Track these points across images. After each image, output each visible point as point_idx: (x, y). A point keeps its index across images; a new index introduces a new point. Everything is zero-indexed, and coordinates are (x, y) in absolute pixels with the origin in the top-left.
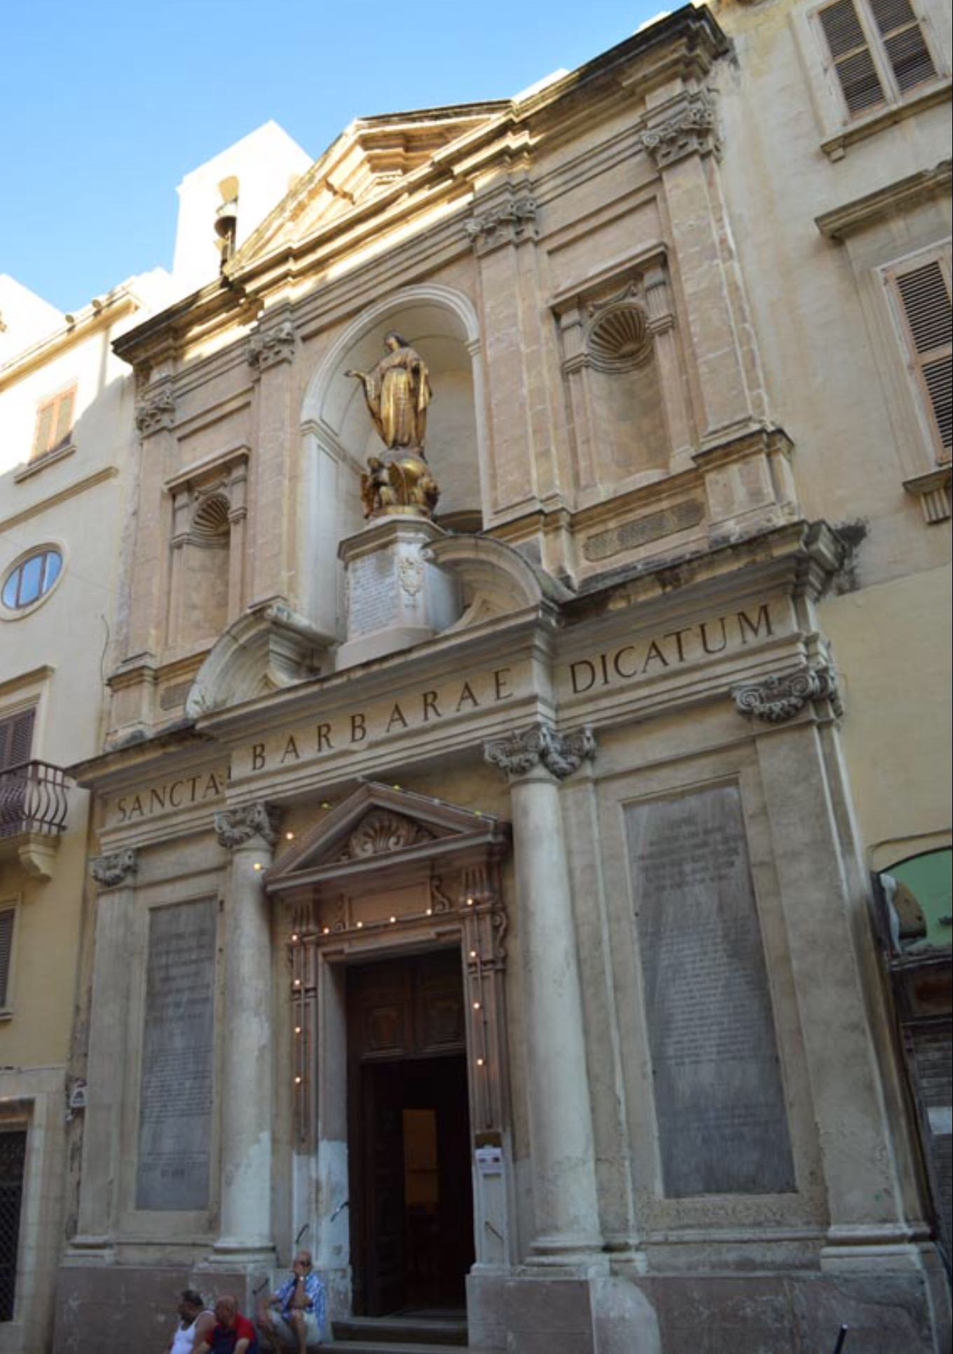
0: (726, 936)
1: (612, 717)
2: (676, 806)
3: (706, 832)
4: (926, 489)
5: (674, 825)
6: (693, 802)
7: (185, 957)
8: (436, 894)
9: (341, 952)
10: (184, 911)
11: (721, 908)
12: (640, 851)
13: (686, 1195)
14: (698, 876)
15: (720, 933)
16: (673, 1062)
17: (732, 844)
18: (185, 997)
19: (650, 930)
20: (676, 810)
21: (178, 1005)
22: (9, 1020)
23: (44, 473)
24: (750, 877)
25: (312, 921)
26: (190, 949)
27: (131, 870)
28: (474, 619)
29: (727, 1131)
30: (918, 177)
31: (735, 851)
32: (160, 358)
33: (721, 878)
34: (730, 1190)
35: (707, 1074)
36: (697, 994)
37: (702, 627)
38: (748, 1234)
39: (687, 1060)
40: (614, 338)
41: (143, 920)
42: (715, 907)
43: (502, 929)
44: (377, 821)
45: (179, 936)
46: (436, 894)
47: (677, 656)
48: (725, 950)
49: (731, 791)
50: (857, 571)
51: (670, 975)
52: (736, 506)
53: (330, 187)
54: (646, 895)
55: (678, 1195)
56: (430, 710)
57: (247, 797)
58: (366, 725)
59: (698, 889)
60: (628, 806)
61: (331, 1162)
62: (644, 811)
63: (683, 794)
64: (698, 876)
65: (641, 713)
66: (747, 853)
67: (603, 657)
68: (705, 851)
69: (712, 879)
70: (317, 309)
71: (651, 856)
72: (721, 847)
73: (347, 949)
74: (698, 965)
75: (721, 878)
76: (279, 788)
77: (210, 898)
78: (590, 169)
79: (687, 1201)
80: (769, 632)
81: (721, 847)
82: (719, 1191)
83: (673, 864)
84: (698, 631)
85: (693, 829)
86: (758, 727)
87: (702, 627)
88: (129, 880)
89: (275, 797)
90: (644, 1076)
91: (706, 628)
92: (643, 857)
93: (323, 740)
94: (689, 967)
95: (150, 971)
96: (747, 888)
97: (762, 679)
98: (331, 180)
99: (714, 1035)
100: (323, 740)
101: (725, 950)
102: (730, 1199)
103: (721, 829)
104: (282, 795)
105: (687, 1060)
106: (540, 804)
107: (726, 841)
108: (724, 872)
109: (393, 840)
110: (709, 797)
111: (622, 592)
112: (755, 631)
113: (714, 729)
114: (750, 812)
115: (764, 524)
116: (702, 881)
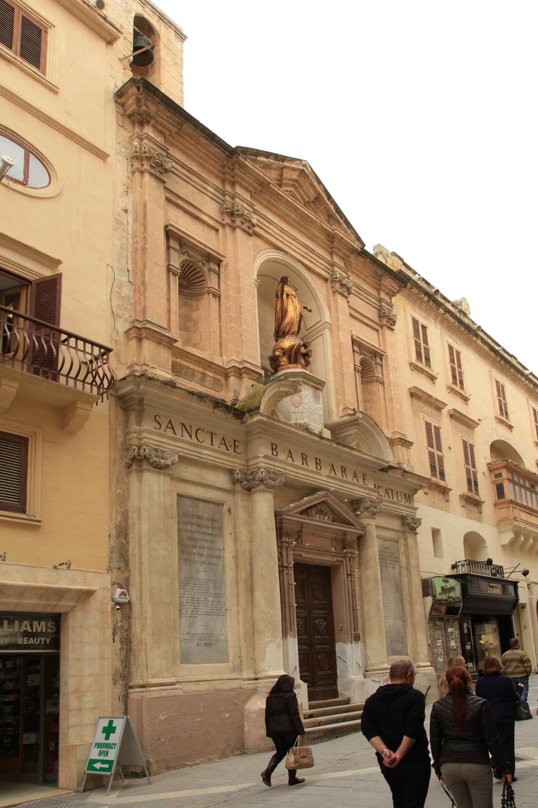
3: (392, 553)
9: (301, 555)
10: (201, 505)
22: (40, 526)
23: (13, 67)
26: (207, 527)
30: (432, 397)
32: (160, 128)
40: (188, 275)
45: (200, 518)
53: (282, 171)
58: (322, 465)
59: (390, 569)
60: (180, 496)
61: (293, 643)
70: (263, 224)
73: (304, 555)
76: (288, 472)
77: (220, 504)
78: (363, 296)
85: (388, 551)
97: (157, 447)
98: (285, 171)
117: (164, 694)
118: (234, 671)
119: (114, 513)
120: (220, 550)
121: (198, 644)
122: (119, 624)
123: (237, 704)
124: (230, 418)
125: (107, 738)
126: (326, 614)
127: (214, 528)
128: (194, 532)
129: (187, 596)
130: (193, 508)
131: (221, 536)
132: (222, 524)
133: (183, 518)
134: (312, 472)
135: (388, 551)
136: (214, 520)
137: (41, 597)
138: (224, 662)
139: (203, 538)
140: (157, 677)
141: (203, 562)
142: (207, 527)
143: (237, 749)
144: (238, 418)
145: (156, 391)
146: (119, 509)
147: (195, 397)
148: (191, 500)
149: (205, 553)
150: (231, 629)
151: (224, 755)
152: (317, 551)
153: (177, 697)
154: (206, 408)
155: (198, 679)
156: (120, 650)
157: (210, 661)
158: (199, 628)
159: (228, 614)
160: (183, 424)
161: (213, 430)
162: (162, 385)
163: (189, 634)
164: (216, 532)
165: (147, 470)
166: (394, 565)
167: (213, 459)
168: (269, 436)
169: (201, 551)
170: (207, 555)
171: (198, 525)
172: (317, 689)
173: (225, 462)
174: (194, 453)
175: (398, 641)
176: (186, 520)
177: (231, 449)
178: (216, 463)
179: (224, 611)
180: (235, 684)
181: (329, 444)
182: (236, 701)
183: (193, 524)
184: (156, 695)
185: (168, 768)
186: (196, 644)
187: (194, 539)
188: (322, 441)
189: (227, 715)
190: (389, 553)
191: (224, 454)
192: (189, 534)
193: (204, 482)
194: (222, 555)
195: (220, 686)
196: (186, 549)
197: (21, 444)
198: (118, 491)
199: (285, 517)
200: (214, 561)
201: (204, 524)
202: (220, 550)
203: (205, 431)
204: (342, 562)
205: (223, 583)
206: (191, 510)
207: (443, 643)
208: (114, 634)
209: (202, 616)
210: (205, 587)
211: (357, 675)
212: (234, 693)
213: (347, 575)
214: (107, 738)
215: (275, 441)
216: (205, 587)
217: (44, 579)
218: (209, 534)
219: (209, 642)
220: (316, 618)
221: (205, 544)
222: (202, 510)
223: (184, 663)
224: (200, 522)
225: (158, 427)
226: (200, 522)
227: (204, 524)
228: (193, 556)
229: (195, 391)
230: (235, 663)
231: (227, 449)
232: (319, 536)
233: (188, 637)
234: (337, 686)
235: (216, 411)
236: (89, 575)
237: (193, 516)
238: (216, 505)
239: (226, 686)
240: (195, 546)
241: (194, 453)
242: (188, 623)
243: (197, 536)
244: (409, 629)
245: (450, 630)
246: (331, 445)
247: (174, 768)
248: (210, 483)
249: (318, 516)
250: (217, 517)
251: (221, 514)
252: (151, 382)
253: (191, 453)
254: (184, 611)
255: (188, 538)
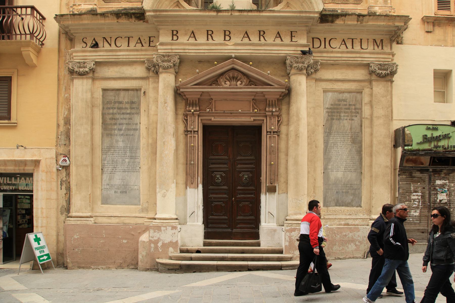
0: (351, 137)
1: (327, 60)
2: (341, 95)
3: (350, 105)
4: (428, 21)
5: (339, 100)
6: (346, 95)
7: (123, 111)
8: (254, 105)
10: (122, 93)
11: (351, 129)
12: (327, 106)
13: (330, 206)
14: (345, 118)
15: (350, 136)
16: (330, 170)
17: (357, 110)
18: (124, 127)
19: (328, 131)
20: (341, 96)
21: (120, 130)
24: (361, 121)
25: (198, 105)
26: (126, 108)
27: (93, 71)
28: (282, 8)
29: (344, 191)
31: (358, 113)
33: (352, 120)
34: (343, 206)
35: (340, 175)
36: (340, 152)
37: (361, 40)
38: (348, 217)
39: (334, 170)
41: (99, 94)
42: (349, 127)
43: (280, 122)
44: (233, 74)
45: (120, 103)
46: (254, 105)
47: (351, 47)
48: (351, 141)
49: (358, 96)
50: (403, 38)
51: (332, 145)
52: (378, 3)
54: (327, 120)
55: (327, 207)
56: (262, 38)
57: (170, 51)
58: (231, 35)
60: (325, 91)
62: (330, 95)
63: (343, 92)
64: (345, 118)
65: (337, 62)
66: (361, 114)
67: (325, 39)
68: (349, 111)
69: (349, 120)
71: (330, 108)
72: (353, 111)
73: (213, 119)
74: (342, 144)
75: (352, 120)
76: (187, 51)
77: (138, 90)
79: (330, 208)
80: (382, 49)
81: (353, 111)
82: (339, 206)
83: (338, 112)
84: (360, 40)
85: (345, 103)
86: (374, 77)
87: (361, 40)
88: (91, 75)
89: (184, 54)
90: (321, 173)
91: (362, 40)
92: (327, 108)
93: (209, 37)
94: (339, 144)
95: (103, 115)
96: (360, 124)
99: (344, 164)
100: (209, 37)
101: (351, 141)
102: (343, 208)
103: (354, 105)
104: (188, 54)
105: (334, 170)
106: (300, 83)
107: (355, 109)
108: (353, 118)
109: (239, 82)
110: (352, 95)
111: (343, 18)
112: (378, 47)
113: (360, 74)
114: (365, 102)
115: (388, 13)
116: (347, 119)
117: (79, 223)
118: (142, 211)
119: (63, 110)
120: (137, 124)
121: (115, 192)
122: (64, 179)
123: (133, 235)
124: (133, 21)
125: (39, 244)
126: (253, 168)
127: (132, 108)
128: (116, 114)
129: (108, 159)
130: (115, 97)
131: (138, 113)
132: (139, 104)
133: (106, 104)
134: (221, 44)
135: (345, 103)
136: (132, 103)
137: (16, 165)
138: (136, 205)
139: (122, 117)
140: (78, 212)
141: (122, 135)
142: (126, 108)
143: (132, 264)
144: (141, 20)
145: (70, 23)
146: (66, 107)
147: (99, 16)
148: (114, 92)
149: (124, 128)
150: (141, 181)
151: (120, 267)
152: (230, 114)
153: (87, 225)
154: (112, 21)
155: (110, 215)
156: (65, 194)
157: (125, 203)
158: (117, 180)
159: (141, 170)
160: (104, 38)
161: (129, 35)
162: (72, 16)
163: (109, 185)
164: (133, 111)
165: (76, 78)
166: (352, 116)
167: (127, 57)
168: (167, 25)
169: (120, 127)
170: (125, 129)
171: (119, 108)
172: (234, 230)
173: (138, 57)
174: (111, 57)
175: (347, 192)
176: (109, 107)
177: (146, 45)
178: (130, 60)
179: (138, 168)
180: (140, 221)
181: (230, 14)
182: (133, 233)
183: (115, 108)
184: (73, 223)
185: (79, 267)
186: (114, 192)
187: (115, 119)
188: (220, 14)
189: (125, 241)
190: (346, 105)
191: (142, 50)
192: (111, 116)
193: (123, 76)
194: (138, 127)
195: (127, 221)
196: (107, 127)
197: (8, 80)
198: (66, 95)
199: (181, 90)
200: (132, 132)
201: (124, 107)
202: (137, 124)
203: (123, 37)
204: (263, 120)
205: (138, 148)
206: (114, 98)
207: (423, 197)
208: (61, 184)
209: (120, 173)
210: (122, 152)
211: (269, 223)
212: (131, 227)
213: (267, 132)
214: (39, 244)
215: (175, 28)
216: (122, 152)
217: (18, 155)
218: (128, 114)
219: (124, 190)
220: (240, 172)
221: (124, 121)
222: (123, 97)
223: (104, 204)
224: (121, 106)
225: (85, 45)
226: (121, 106)
227: (124, 107)
228: (113, 131)
229: (121, 9)
230: (144, 206)
231: (143, 46)
232: (233, 100)
233: (108, 187)
234: (259, 230)
235: (120, 20)
236: (42, 151)
237: (115, 102)
238: (135, 91)
239: (133, 221)
240: (115, 124)
241: (111, 57)
242: (108, 177)
243: (117, 116)
244: (366, 182)
245: (438, 182)
246: (231, 14)
247: (83, 268)
248: (128, 75)
249: (228, 83)
250: (136, 100)
251: (139, 97)
252: (64, 17)
253: (109, 57)
254: (106, 170)
255: (110, 119)
